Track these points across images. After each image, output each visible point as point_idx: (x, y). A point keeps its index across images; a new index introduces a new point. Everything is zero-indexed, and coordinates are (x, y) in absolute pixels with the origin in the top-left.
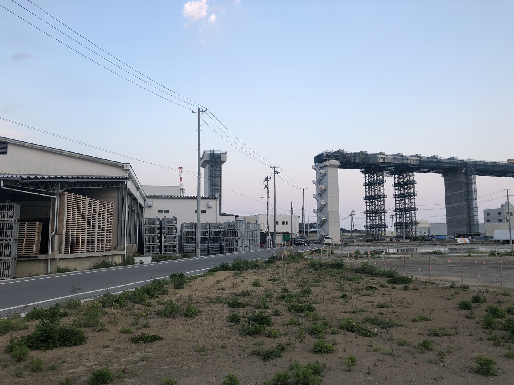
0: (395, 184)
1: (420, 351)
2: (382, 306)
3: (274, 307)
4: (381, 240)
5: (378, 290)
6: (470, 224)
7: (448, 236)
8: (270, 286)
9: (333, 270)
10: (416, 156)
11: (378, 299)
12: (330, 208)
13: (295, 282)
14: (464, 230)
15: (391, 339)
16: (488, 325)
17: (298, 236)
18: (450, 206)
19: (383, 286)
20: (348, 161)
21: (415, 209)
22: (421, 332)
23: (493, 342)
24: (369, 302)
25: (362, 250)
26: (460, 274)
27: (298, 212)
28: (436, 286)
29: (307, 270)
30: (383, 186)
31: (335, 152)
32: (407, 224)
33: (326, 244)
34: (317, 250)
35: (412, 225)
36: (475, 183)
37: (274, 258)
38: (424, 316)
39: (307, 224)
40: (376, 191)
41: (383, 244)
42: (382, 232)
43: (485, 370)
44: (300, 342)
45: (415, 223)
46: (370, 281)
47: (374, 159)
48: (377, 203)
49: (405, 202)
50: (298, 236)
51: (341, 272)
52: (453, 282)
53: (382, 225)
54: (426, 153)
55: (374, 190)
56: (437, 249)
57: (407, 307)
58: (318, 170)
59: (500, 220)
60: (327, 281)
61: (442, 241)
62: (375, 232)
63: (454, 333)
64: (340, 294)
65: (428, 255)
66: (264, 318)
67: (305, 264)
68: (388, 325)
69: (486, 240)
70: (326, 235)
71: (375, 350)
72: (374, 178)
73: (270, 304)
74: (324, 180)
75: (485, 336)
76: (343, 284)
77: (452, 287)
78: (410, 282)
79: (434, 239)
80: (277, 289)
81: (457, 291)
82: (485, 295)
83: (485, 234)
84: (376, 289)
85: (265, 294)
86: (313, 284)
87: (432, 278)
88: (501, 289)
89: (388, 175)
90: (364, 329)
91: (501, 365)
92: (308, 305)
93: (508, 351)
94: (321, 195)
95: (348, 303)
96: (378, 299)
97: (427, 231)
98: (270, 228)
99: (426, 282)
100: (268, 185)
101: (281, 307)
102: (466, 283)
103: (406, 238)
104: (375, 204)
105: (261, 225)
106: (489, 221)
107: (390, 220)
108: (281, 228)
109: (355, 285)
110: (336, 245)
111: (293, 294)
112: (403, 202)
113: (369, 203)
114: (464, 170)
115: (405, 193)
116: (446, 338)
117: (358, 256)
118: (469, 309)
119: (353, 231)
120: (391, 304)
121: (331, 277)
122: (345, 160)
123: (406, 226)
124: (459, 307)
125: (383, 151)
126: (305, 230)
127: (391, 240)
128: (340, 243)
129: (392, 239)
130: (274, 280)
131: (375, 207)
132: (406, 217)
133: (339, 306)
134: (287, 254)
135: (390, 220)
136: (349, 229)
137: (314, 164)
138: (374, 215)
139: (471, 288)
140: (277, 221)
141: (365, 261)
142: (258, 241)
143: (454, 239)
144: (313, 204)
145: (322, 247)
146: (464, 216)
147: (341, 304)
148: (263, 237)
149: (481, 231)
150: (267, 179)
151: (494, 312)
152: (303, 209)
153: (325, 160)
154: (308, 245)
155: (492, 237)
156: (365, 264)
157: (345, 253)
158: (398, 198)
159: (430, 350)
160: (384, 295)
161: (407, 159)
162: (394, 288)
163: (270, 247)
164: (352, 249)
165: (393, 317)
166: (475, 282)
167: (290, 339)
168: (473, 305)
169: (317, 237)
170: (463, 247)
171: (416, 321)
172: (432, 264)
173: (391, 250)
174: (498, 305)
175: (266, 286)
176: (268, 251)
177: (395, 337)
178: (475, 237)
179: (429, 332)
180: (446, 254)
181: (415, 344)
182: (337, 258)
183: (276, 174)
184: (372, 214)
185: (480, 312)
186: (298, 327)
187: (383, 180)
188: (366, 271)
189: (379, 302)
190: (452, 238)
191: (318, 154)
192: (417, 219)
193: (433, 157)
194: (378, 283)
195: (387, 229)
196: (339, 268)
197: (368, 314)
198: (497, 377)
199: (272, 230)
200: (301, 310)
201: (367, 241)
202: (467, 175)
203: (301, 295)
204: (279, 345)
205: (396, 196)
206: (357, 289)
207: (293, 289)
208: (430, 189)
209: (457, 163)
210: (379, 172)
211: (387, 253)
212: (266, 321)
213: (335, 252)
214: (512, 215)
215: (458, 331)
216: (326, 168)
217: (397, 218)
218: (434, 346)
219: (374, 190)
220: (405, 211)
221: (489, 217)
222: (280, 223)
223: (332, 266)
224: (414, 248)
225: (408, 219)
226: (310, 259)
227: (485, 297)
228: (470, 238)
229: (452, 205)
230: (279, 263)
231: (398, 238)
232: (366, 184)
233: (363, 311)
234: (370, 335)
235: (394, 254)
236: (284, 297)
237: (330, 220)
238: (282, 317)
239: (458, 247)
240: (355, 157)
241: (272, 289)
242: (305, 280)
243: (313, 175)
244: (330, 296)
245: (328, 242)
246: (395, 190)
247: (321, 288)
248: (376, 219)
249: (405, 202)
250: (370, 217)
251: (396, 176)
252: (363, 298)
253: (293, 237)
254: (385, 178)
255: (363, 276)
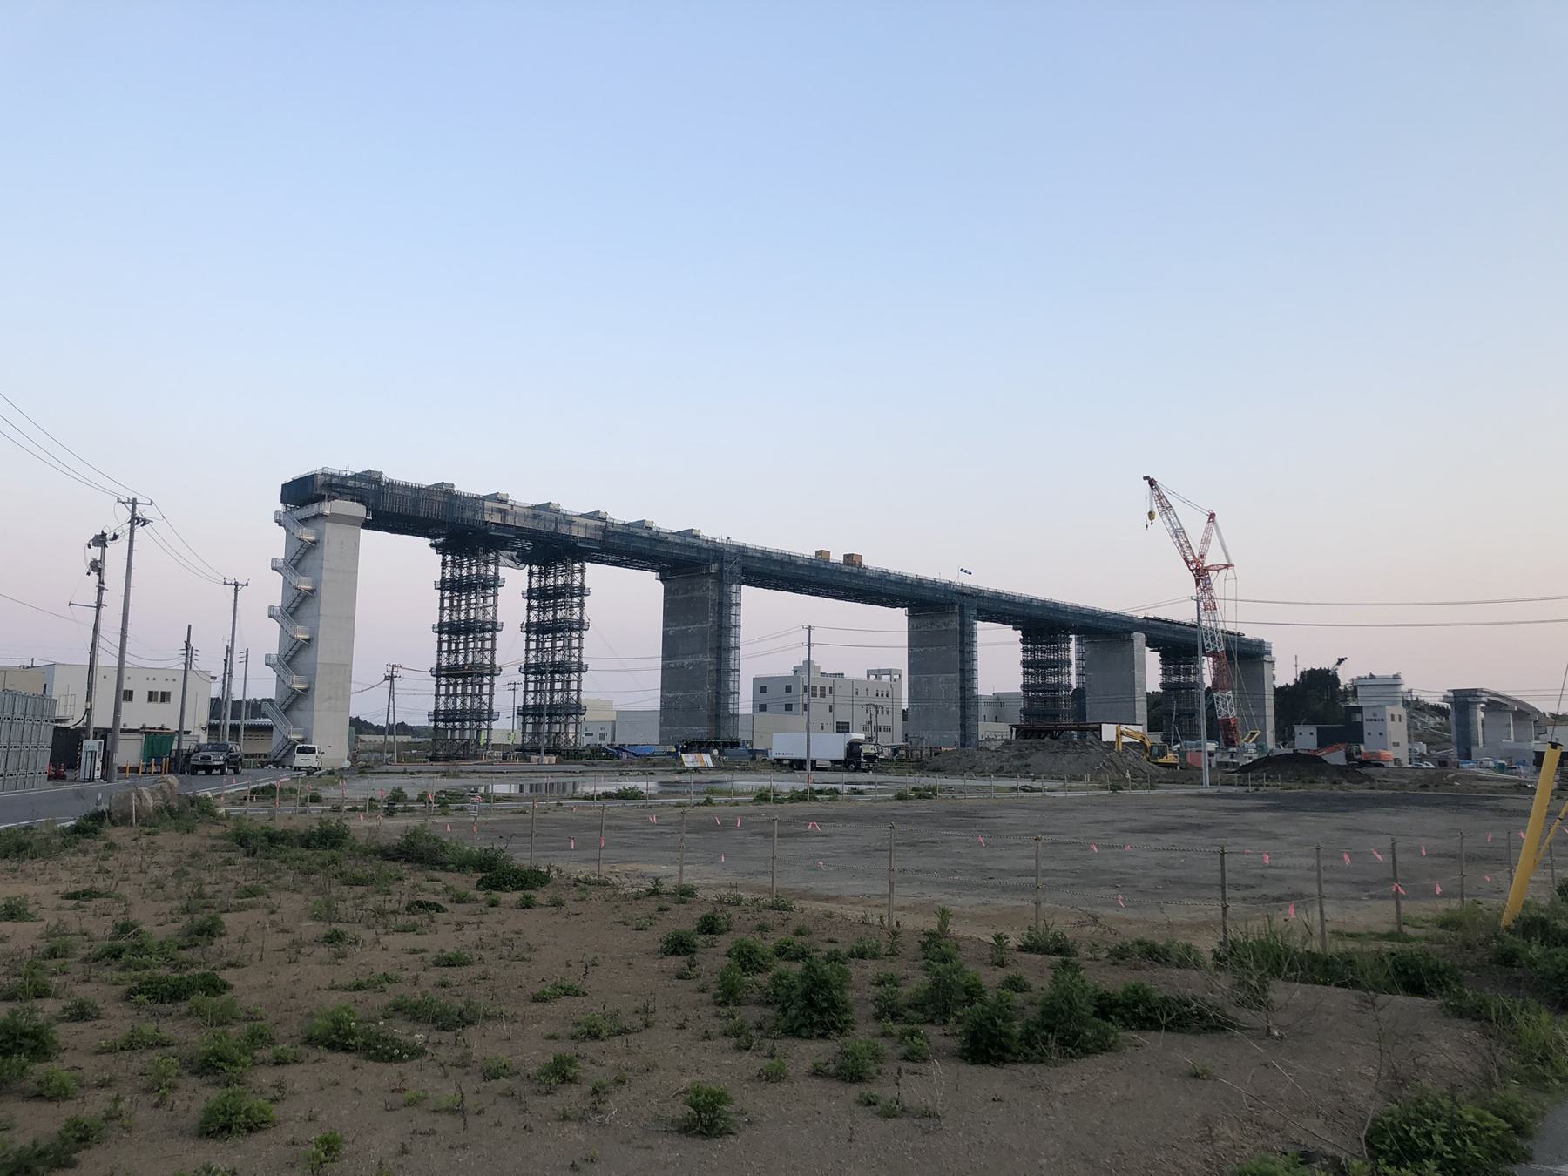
0: (530, 590)
1: (543, 1088)
2: (450, 962)
3: (76, 989)
4: (476, 757)
5: (445, 910)
6: (718, 716)
7: (661, 749)
8: (69, 916)
9: (309, 853)
10: (594, 516)
11: (441, 938)
12: (324, 653)
13: (168, 899)
14: (702, 732)
15: (463, 1063)
16: (728, 995)
17: (204, 739)
18: (673, 663)
19: (460, 900)
20: (393, 508)
21: (581, 669)
22: (552, 1032)
23: (734, 1040)
24: (414, 952)
25: (412, 788)
26: (678, 855)
27: (209, 660)
28: (610, 892)
29: (218, 858)
30: (495, 595)
31: (354, 477)
32: (554, 712)
33: (298, 769)
34: (263, 790)
35: (568, 715)
36: (738, 604)
37: (99, 817)
38: (567, 984)
39: (239, 702)
40: (471, 608)
41: (478, 768)
42: (479, 732)
43: (706, 1122)
44: (157, 1106)
45: (578, 709)
46: (425, 884)
47: (475, 511)
48: (471, 645)
49: (553, 647)
50: (204, 739)
51: (333, 861)
52: (657, 880)
53: (481, 712)
54: (622, 513)
55: (468, 604)
56: (628, 785)
57: (523, 959)
58: (294, 529)
59: (788, 707)
60: (286, 889)
61: (643, 760)
62: (459, 733)
63: (639, 1023)
64: (321, 929)
65: (599, 803)
66: (24, 1035)
67: (219, 837)
68: (458, 1021)
69: (753, 759)
70: (302, 741)
71: (410, 1103)
72: (469, 568)
73: (56, 979)
74: (308, 563)
75: (716, 1026)
76: (338, 899)
77: (654, 893)
78: (542, 884)
79: (625, 756)
80: (98, 926)
81: (665, 904)
82: (731, 910)
83: (751, 742)
84: (439, 909)
85: (44, 946)
86: (235, 902)
87: (605, 868)
88: (770, 891)
89: (511, 563)
90: (385, 1040)
91: (747, 1099)
92: (204, 975)
93: (767, 1062)
94: (296, 609)
95: (344, 957)
96: (441, 938)
97: (608, 731)
98: (95, 712)
99: (587, 882)
100: (102, 561)
101: (101, 990)
102: (688, 880)
103: (547, 753)
104: (466, 648)
105: (61, 702)
106: (763, 708)
107: (507, 696)
108: (139, 714)
109: (374, 900)
110: (330, 773)
111: (154, 941)
112: (548, 645)
113: (449, 643)
114: (714, 568)
115: (555, 617)
116: (618, 1042)
117: (399, 806)
118: (687, 952)
119: (390, 727)
120: (476, 954)
121: (300, 877)
122: (386, 504)
123: (549, 715)
124: (662, 950)
125: (502, 491)
126: (229, 722)
127: (504, 758)
128: (347, 764)
129: (507, 753)
130: (89, 894)
131: (465, 658)
132: (552, 690)
133: (315, 969)
134: (151, 803)
135: (507, 696)
136: (380, 721)
137: (281, 507)
138: (460, 681)
139: (700, 894)
140: (126, 686)
141: (414, 822)
142: (46, 756)
143: (676, 755)
144: (265, 638)
145: (284, 779)
146: (707, 691)
147: (321, 963)
148: (67, 747)
149: (743, 735)
150: (101, 541)
151: (747, 959)
152: (230, 651)
153: (321, 498)
154: (237, 772)
155: (766, 752)
156: (415, 833)
157: (358, 797)
158: (535, 632)
159: (573, 1080)
160: (460, 926)
161: (570, 523)
162: (494, 904)
163: (92, 780)
164: (380, 786)
165: (481, 998)
166: (710, 877)
167: (117, 1100)
168: (700, 940)
169: (270, 746)
170: (696, 777)
171: (544, 1000)
172: (609, 827)
173: (500, 789)
174: (758, 936)
175: (51, 920)
176: (79, 795)
177: (476, 1054)
178: (728, 750)
179: (575, 1030)
180: (651, 797)
181: (532, 1070)
182: (332, 815)
183: (138, 528)
184: (456, 676)
185: (714, 958)
186: (154, 1055)
187: (496, 577)
188: (416, 853)
189: (442, 951)
190: (670, 753)
191: (296, 476)
192: (583, 696)
193: (641, 524)
194: (447, 889)
195: (494, 725)
196: (332, 846)
197: (405, 990)
198: (732, 1139)
199: (103, 720)
200: (176, 993)
201: (433, 759)
202: (719, 578)
203: (186, 942)
204: (74, 1124)
205: (528, 628)
206: (380, 912)
207: (157, 922)
208: (624, 612)
209: (699, 549)
210: (486, 552)
211: (487, 798)
212: (34, 1043)
213: (324, 795)
214: (814, 695)
215: (652, 1018)
216: (319, 524)
217: (526, 691)
218: (583, 1069)
219: (468, 604)
220: (552, 673)
221: (763, 699)
222: (140, 696)
223: (308, 841)
224: (569, 780)
225: (557, 697)
226: (238, 818)
227: (729, 916)
228: (716, 752)
229: (678, 662)
230: (116, 834)
231: (525, 752)
232: (443, 585)
233: (388, 980)
234: (401, 1055)
235: (508, 798)
236: (115, 954)
237: (319, 691)
238: (99, 1023)
239: (683, 778)
240: (416, 500)
241: (75, 928)
242: (208, 890)
243: (276, 542)
244: (285, 940)
245: (307, 764)
246: (530, 608)
247: (259, 915)
248: (464, 694)
249: (553, 647)
250: (447, 686)
251: (535, 568)
252: (397, 941)
253: (185, 746)
254: (504, 572)
255: (403, 868)
